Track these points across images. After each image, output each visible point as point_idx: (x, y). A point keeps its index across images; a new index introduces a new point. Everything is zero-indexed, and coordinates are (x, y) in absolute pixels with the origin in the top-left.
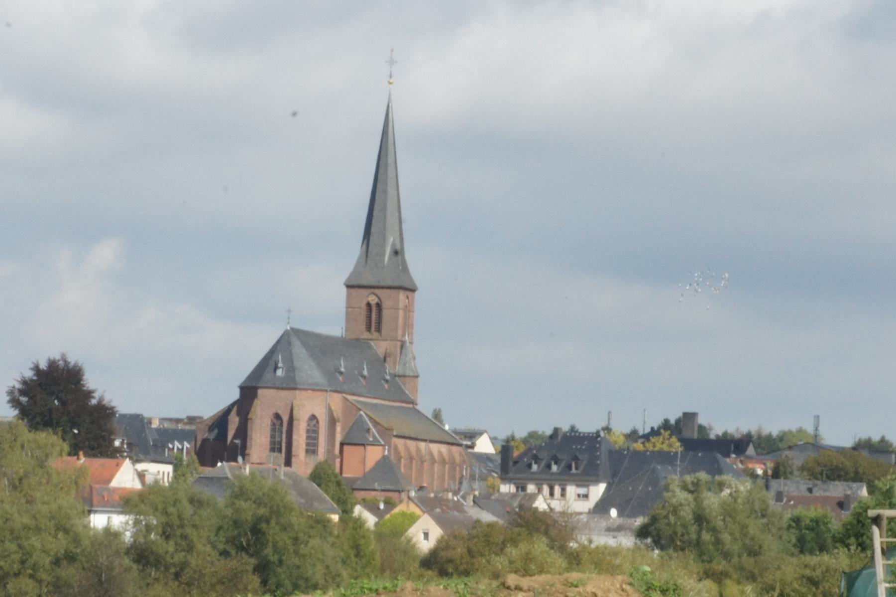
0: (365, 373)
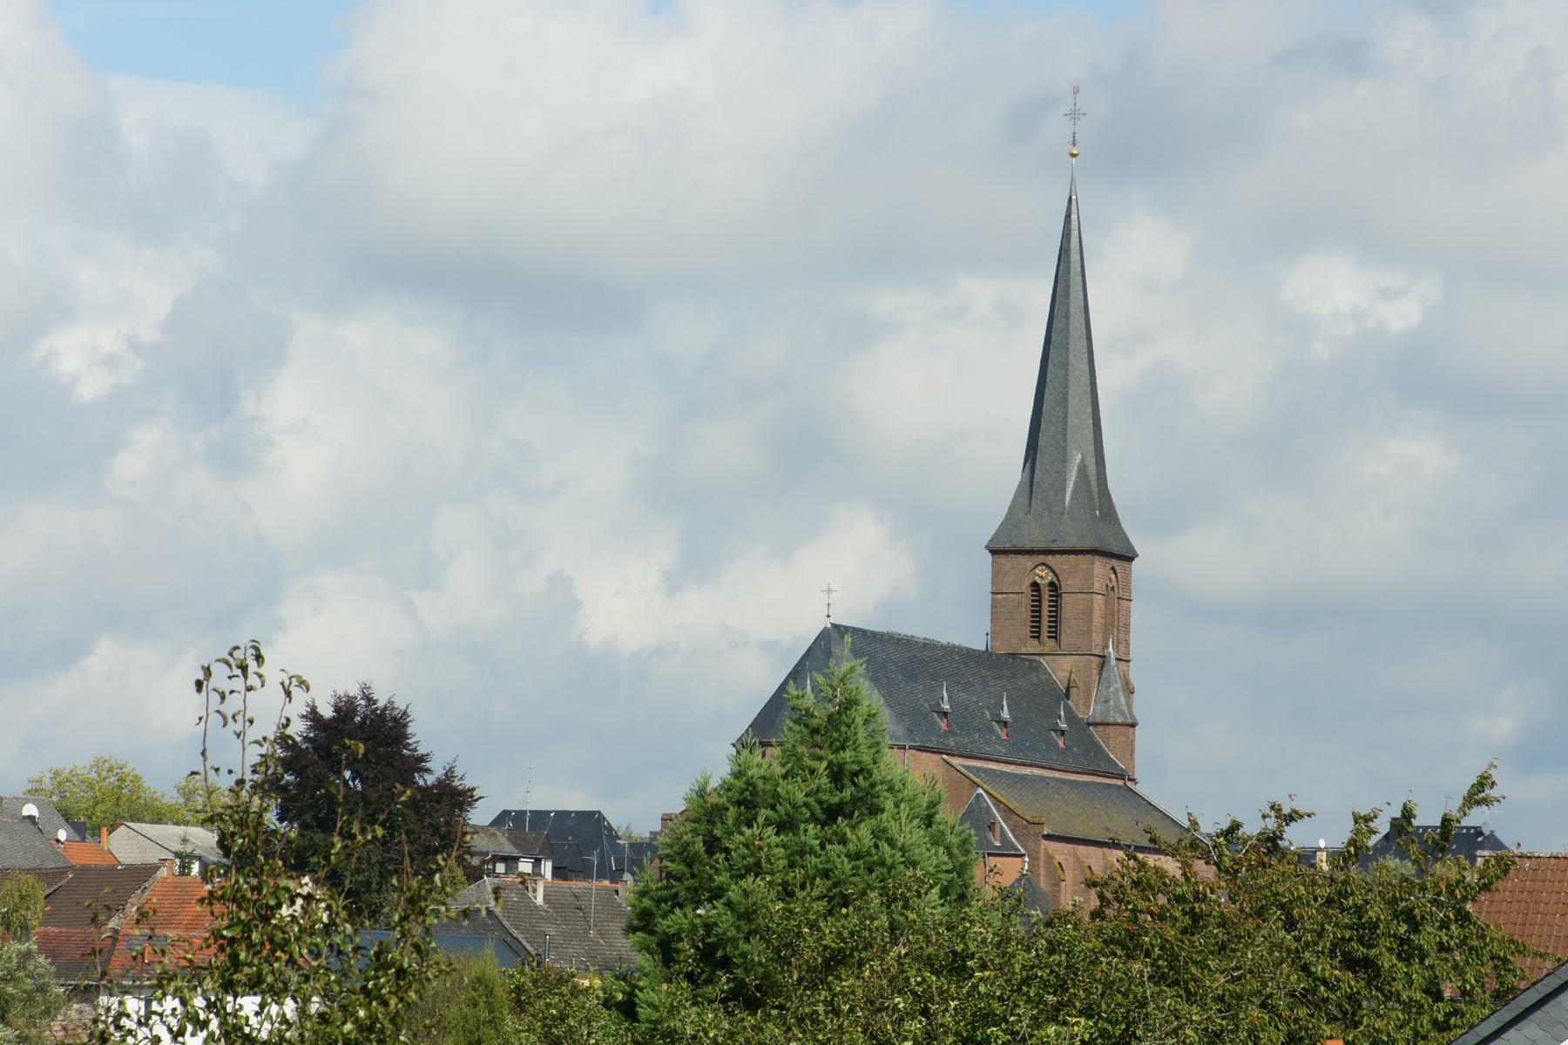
0: (1006, 715)
